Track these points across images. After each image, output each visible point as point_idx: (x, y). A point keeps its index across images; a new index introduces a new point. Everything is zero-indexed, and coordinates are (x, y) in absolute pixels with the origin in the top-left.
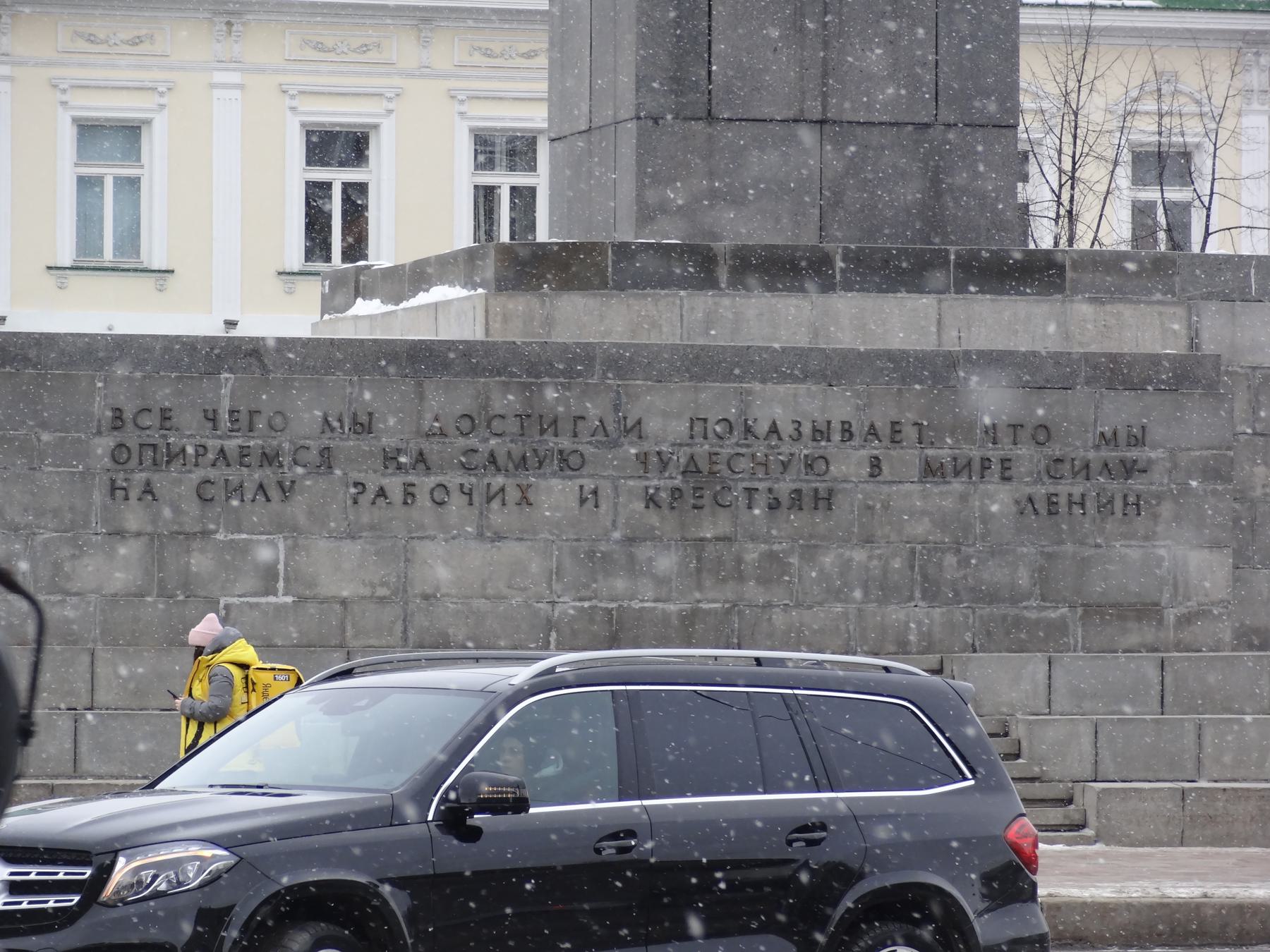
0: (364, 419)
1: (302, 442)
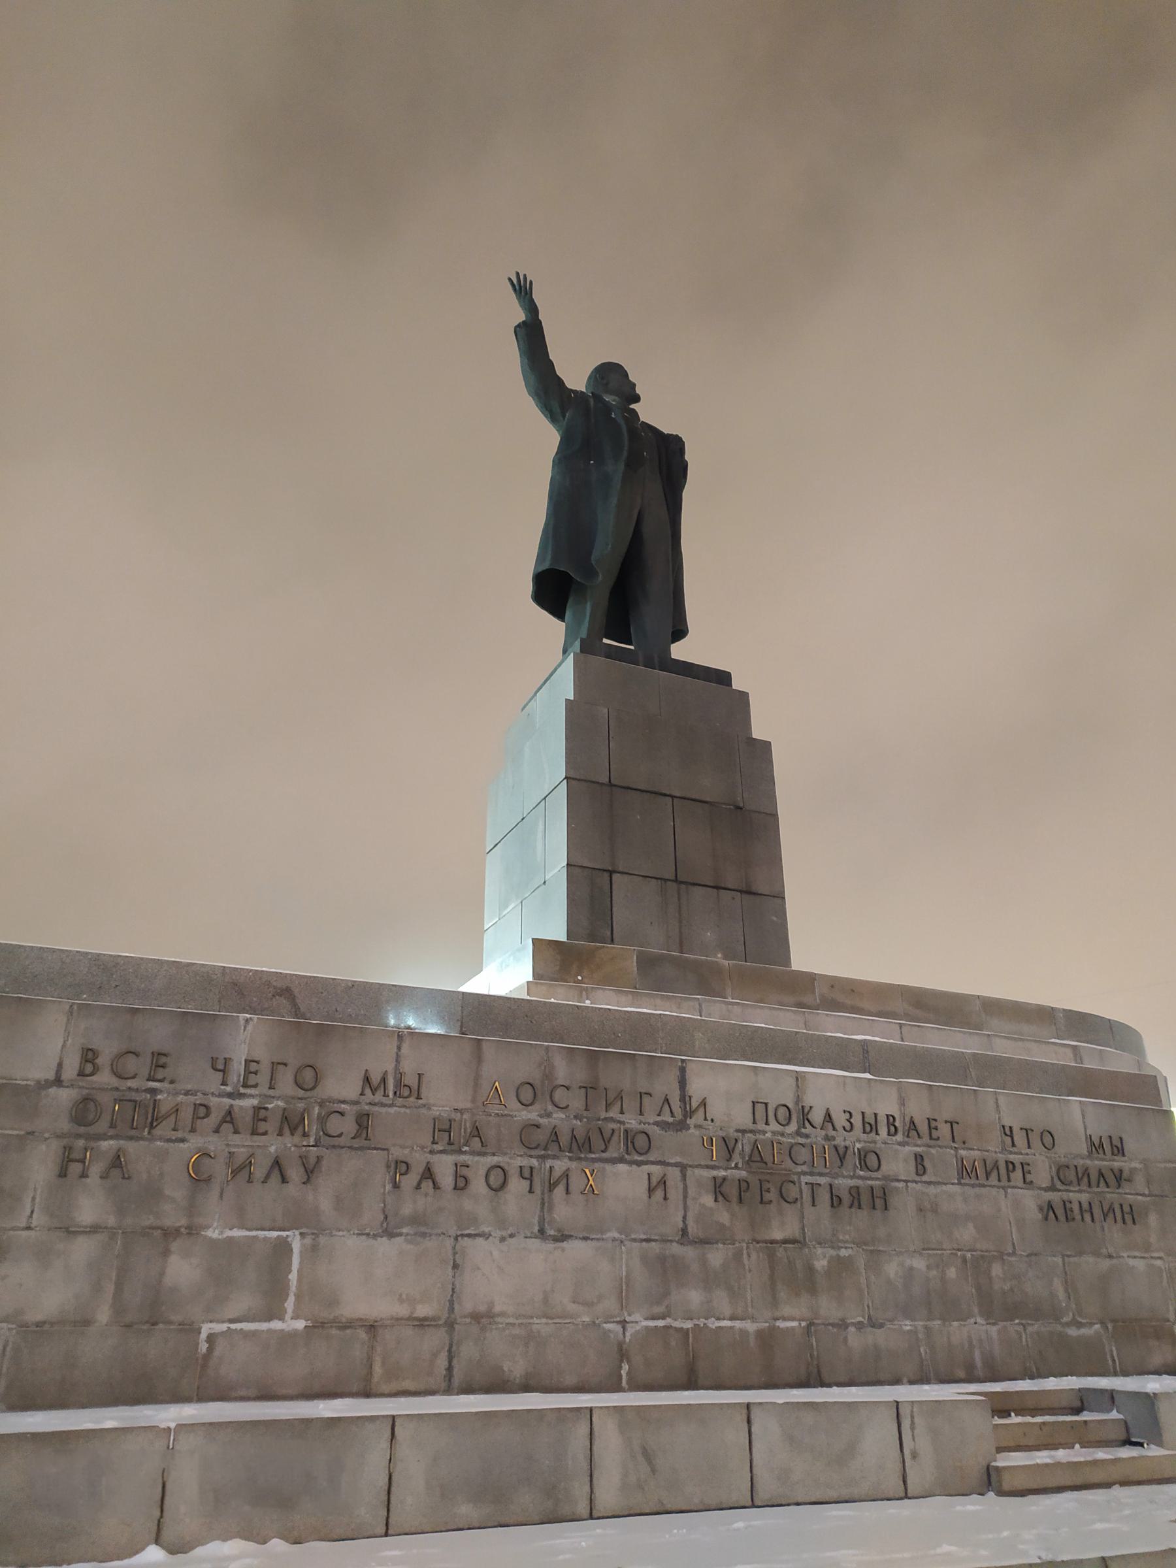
1: (336, 1107)
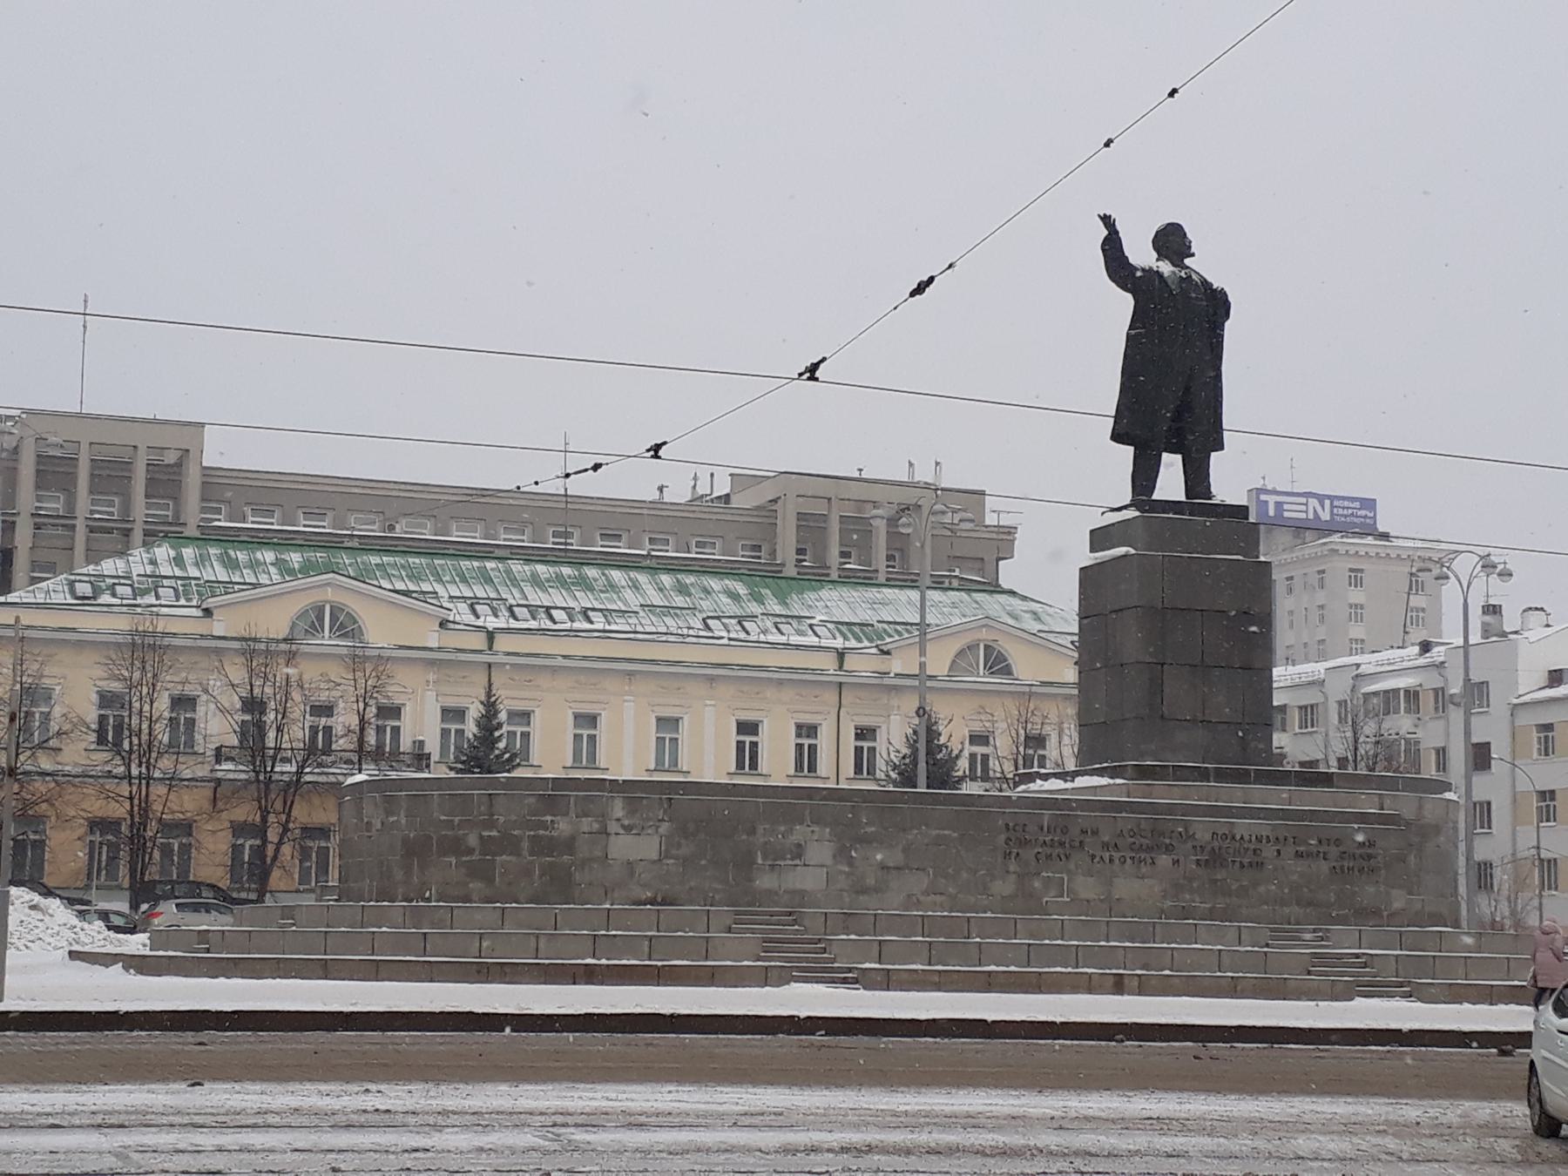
0: (1095, 830)
